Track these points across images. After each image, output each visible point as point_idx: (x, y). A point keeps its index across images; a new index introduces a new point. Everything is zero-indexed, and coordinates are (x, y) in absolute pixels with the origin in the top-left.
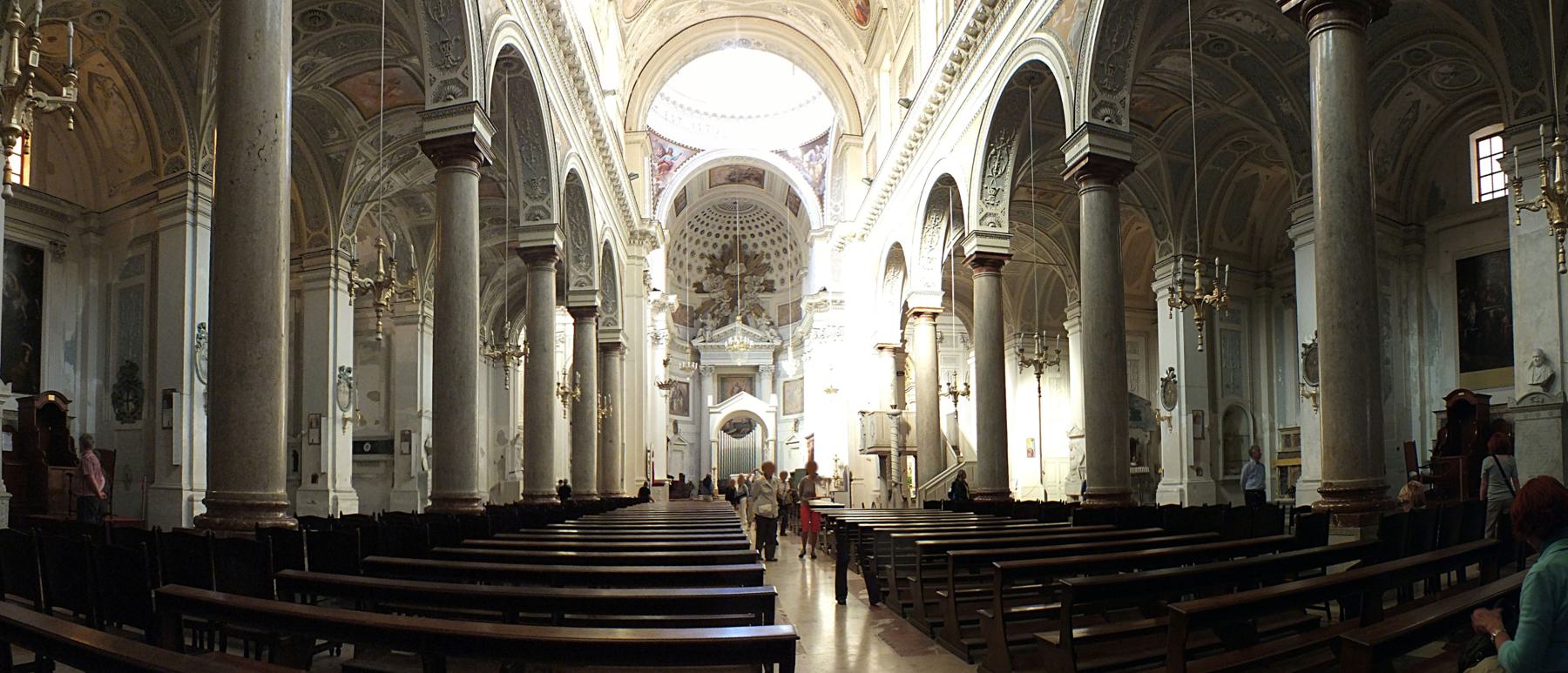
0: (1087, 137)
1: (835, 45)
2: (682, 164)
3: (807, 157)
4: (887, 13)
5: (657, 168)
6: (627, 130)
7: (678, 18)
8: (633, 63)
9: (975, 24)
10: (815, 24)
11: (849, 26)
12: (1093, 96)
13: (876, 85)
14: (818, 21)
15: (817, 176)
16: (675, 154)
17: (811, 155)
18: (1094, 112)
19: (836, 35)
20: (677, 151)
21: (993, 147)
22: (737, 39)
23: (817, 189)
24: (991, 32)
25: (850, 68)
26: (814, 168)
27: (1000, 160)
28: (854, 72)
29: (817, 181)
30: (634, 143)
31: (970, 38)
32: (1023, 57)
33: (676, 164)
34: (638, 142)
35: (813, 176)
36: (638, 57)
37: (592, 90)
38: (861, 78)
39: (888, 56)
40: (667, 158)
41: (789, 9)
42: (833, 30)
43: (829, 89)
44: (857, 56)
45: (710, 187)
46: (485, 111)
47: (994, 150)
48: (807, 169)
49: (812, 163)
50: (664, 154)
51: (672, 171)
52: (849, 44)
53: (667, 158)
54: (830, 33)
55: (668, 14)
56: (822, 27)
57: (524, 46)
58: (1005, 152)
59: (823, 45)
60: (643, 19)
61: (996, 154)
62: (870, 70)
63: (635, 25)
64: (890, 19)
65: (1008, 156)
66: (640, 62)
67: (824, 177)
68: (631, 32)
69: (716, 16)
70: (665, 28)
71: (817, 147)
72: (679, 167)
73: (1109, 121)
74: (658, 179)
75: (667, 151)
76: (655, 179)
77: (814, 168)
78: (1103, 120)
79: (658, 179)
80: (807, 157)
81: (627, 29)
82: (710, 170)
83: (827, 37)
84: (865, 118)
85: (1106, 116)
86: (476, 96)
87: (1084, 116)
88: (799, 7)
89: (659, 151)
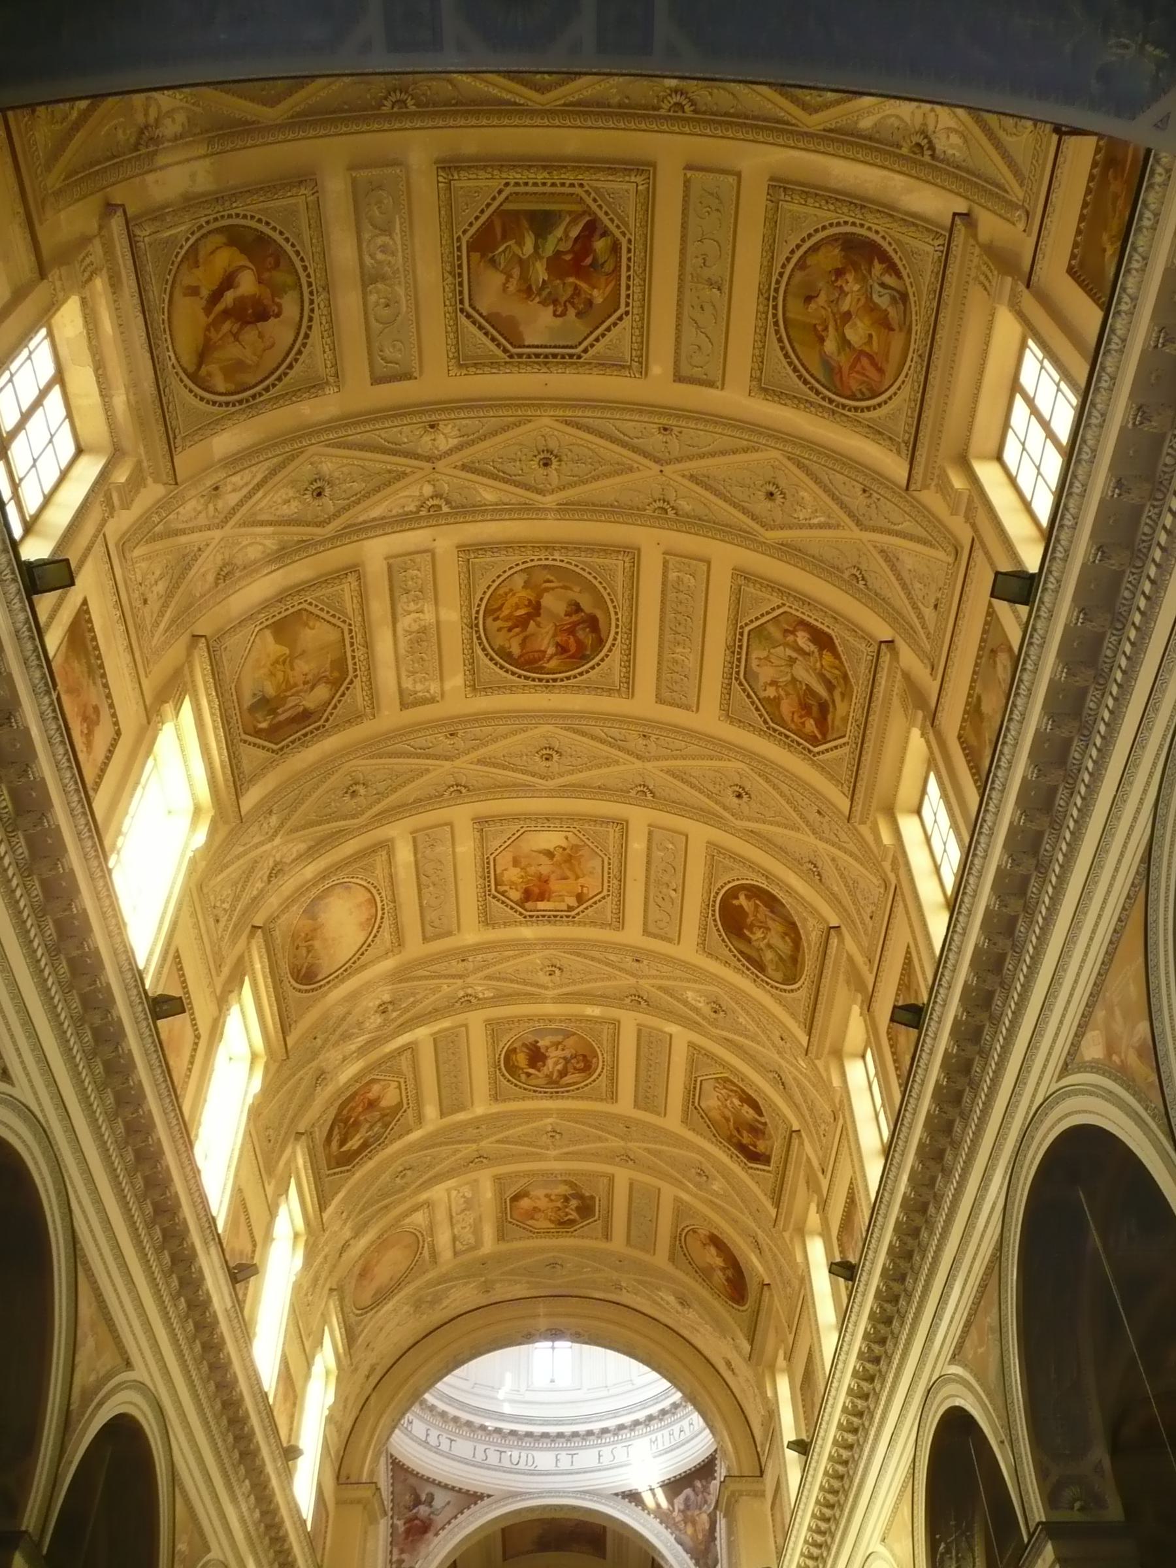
0: (1049, 1548)
1: (702, 1330)
2: (449, 1523)
3: (679, 1502)
4: (770, 1289)
5: (402, 1529)
6: (343, 1480)
7: (445, 1303)
8: (364, 1369)
9: (869, 1348)
10: (668, 1303)
11: (718, 1305)
12: (1042, 1473)
13: (770, 1394)
14: (671, 1299)
15: (700, 1537)
16: (438, 1502)
17: (687, 1499)
18: (1052, 1499)
19: (701, 1317)
20: (440, 1499)
21: (940, 1541)
22: (543, 1329)
23: (701, 1562)
24: (897, 1357)
25: (728, 1364)
26: (694, 1523)
27: (958, 1561)
28: (736, 1371)
29: (702, 1547)
30: (351, 1503)
31: (868, 1366)
32: (939, 1406)
33: (439, 1520)
34: (359, 1502)
35: (694, 1537)
36: (374, 1361)
37: (265, 1452)
38: (748, 1380)
39: (781, 1354)
40: (423, 1510)
41: (624, 1284)
42: (694, 1310)
43: (699, 1398)
44: (737, 1348)
45: (505, 1559)
46: (39, 1545)
47: (942, 1546)
48: (682, 1526)
49: (689, 1513)
50: (417, 1502)
51: (430, 1535)
52: (721, 1329)
53: (423, 1510)
54: (691, 1315)
55: (429, 1299)
56: (679, 1308)
57: (152, 1421)
58: (964, 1545)
59: (685, 1333)
60: (389, 1306)
61: (948, 1550)
62: (760, 1369)
63: (371, 1318)
64: (776, 1298)
65: (972, 1551)
66: (378, 1368)
67: (714, 1539)
68: (365, 1327)
69: (509, 1297)
70: (425, 1317)
71: (698, 1484)
72: (443, 1528)
73: (1081, 1509)
74: (402, 1551)
75: (423, 1497)
76: (395, 1551)
77: (694, 1523)
78: (1072, 1508)
79: (402, 1551)
80: (679, 1502)
81: (359, 1323)
82: (503, 1530)
83: (688, 1321)
84: (763, 1445)
85: (1075, 1500)
86: (30, 1520)
87: (1038, 1513)
88: (640, 1282)
89: (408, 1498)
